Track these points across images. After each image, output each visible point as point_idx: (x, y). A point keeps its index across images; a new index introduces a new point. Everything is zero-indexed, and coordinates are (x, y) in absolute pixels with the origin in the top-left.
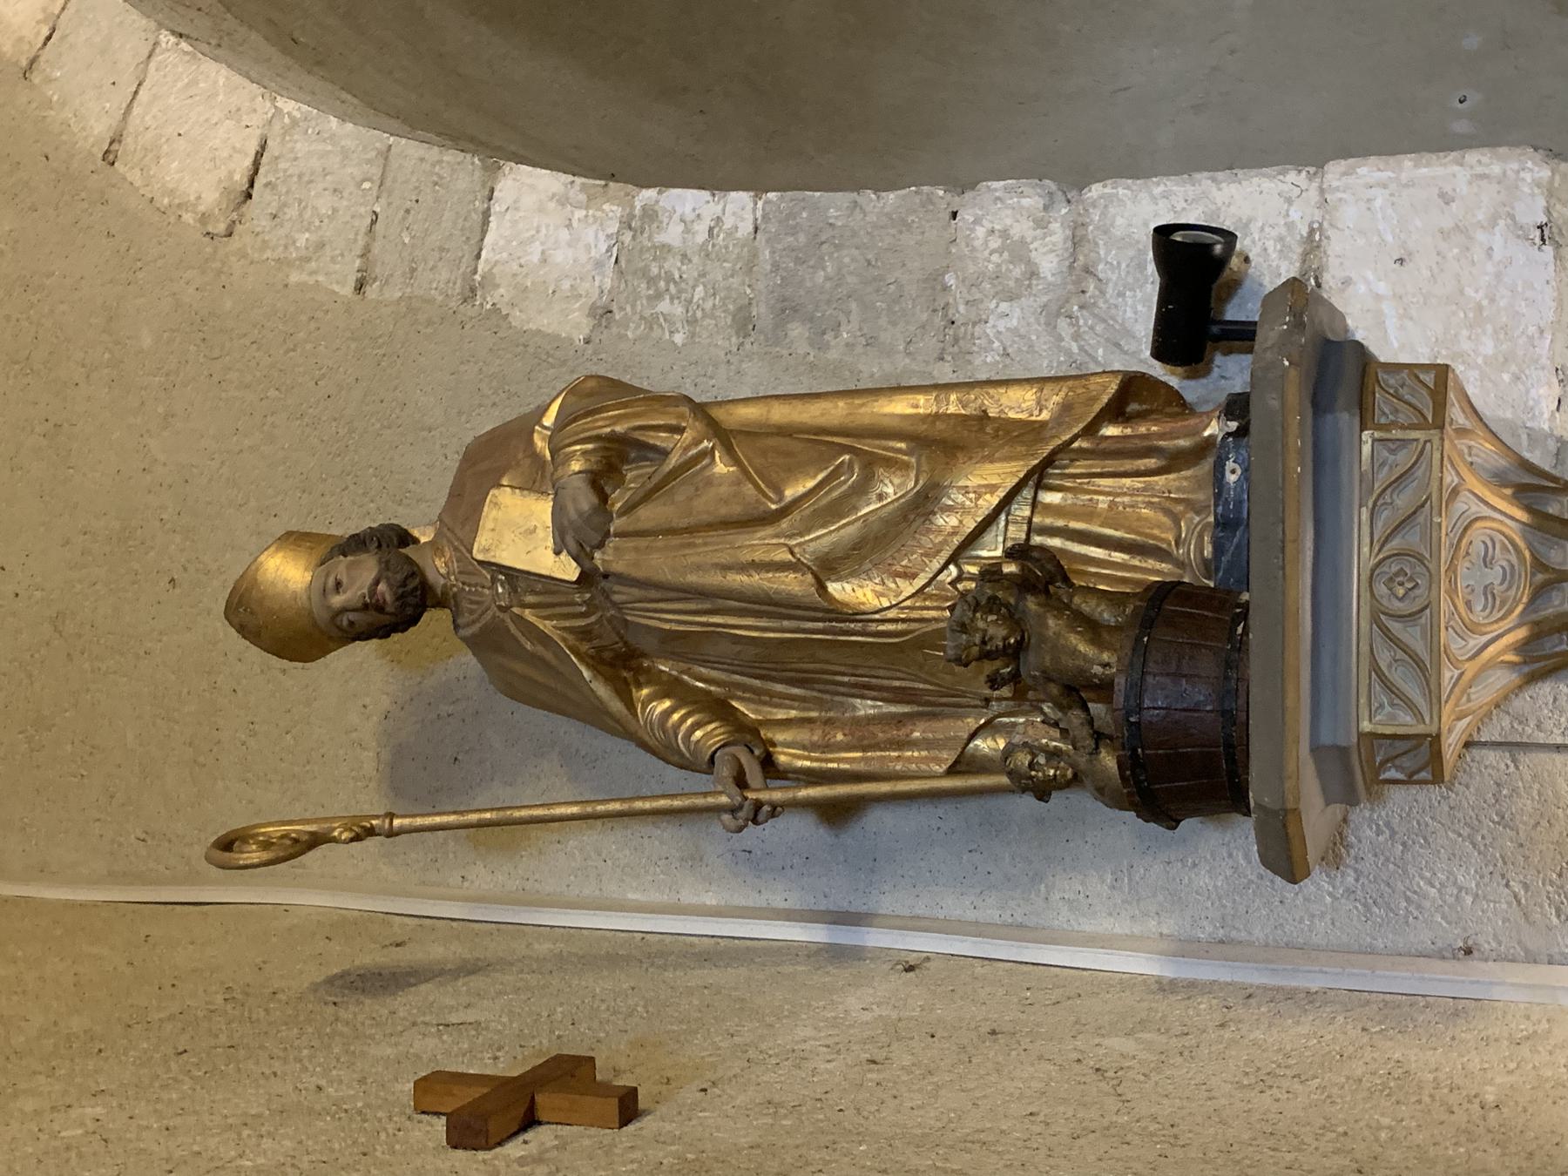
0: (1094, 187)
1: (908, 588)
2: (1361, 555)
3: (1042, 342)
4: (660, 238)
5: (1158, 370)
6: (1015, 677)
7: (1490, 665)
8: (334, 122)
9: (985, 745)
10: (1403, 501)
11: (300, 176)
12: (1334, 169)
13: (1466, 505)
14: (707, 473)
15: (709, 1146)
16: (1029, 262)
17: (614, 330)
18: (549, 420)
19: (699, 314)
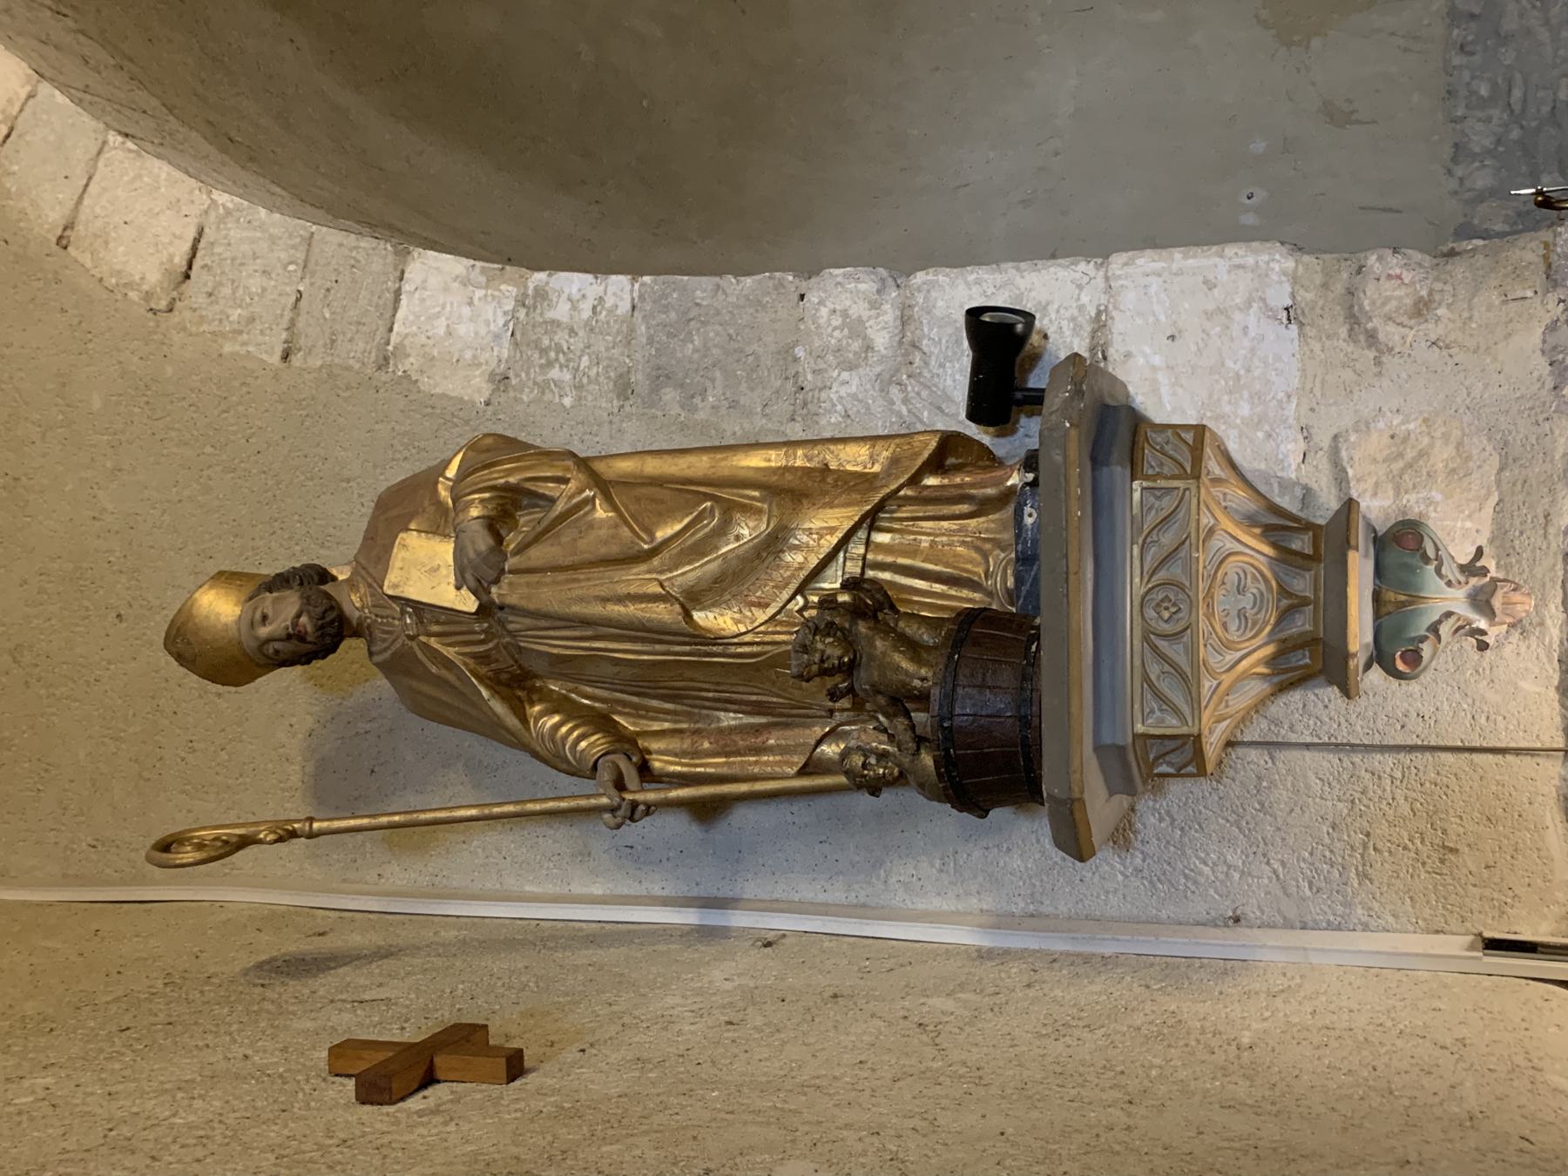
0: (919, 274)
1: (762, 616)
2: (1133, 585)
3: (878, 407)
4: (550, 315)
5: (973, 430)
6: (851, 690)
7: (1246, 676)
8: (263, 212)
9: (830, 750)
10: (1168, 539)
11: (233, 259)
12: (1117, 260)
13: (1220, 542)
14: (589, 518)
15: (583, 1096)
16: (865, 338)
17: (512, 394)
18: (451, 472)
19: (585, 380)
